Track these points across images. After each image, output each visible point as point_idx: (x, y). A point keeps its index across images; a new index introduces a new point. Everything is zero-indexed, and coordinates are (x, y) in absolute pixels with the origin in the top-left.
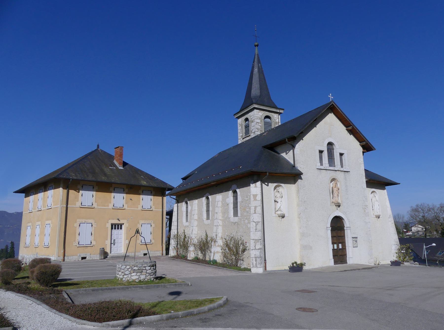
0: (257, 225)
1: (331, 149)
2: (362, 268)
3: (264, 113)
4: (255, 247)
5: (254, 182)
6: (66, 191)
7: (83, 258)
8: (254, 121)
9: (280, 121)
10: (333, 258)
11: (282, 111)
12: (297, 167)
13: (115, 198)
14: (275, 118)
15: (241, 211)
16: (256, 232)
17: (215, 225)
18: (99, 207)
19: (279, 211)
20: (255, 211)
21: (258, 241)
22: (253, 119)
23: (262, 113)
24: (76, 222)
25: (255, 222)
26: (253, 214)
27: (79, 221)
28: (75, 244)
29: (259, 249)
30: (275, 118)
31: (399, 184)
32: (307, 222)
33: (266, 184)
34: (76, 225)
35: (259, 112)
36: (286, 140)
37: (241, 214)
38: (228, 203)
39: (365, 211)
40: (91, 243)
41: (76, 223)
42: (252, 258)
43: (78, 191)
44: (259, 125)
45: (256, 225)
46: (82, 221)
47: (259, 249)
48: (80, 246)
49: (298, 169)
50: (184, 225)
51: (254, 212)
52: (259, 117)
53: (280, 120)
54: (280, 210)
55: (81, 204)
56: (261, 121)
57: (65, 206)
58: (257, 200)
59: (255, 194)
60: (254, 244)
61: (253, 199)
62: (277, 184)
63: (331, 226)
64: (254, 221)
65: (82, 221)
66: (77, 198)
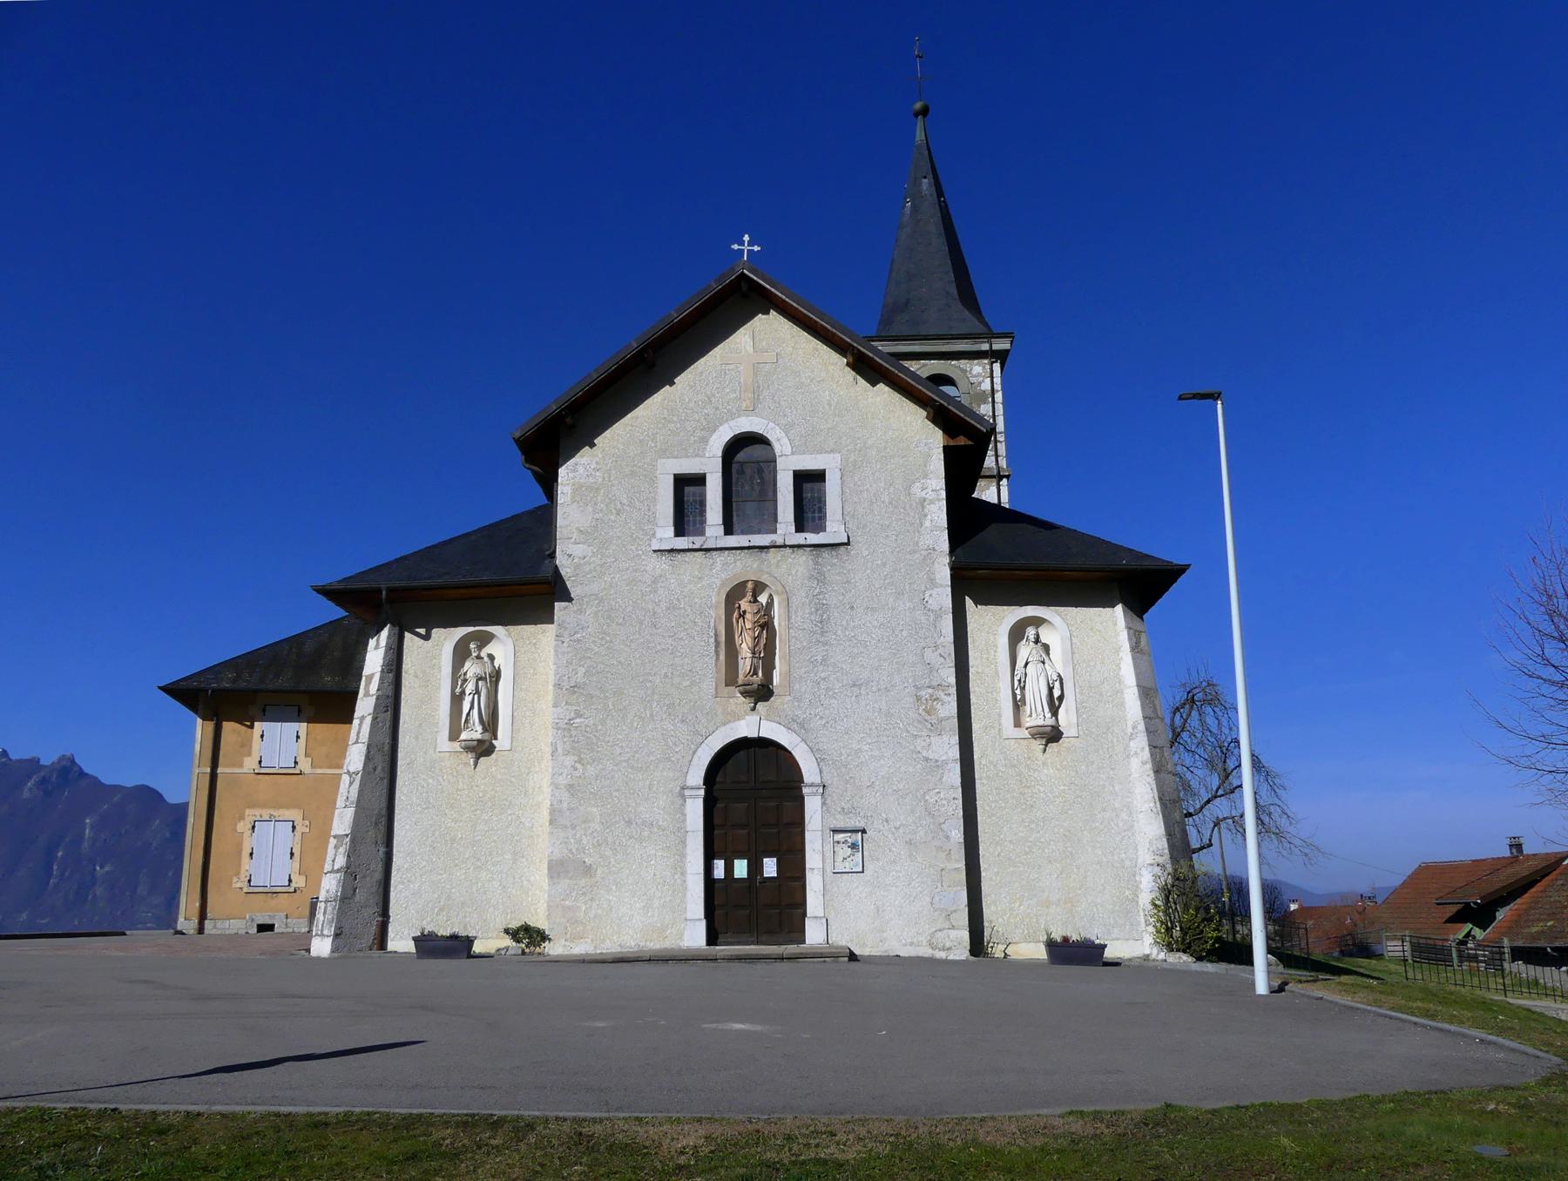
1: (758, 462)
2: (1316, 991)
6: (210, 725)
7: (265, 928)
9: (998, 387)
11: (1001, 345)
13: (264, 738)
14: (975, 376)
18: (319, 771)
24: (242, 818)
27: (251, 814)
28: (239, 885)
30: (975, 376)
33: (418, 635)
34: (244, 826)
40: (290, 881)
41: (242, 822)
43: (248, 723)
46: (261, 816)
48: (255, 892)
53: (998, 380)
55: (260, 762)
57: (209, 770)
62: (471, 629)
65: (261, 816)
66: (246, 747)
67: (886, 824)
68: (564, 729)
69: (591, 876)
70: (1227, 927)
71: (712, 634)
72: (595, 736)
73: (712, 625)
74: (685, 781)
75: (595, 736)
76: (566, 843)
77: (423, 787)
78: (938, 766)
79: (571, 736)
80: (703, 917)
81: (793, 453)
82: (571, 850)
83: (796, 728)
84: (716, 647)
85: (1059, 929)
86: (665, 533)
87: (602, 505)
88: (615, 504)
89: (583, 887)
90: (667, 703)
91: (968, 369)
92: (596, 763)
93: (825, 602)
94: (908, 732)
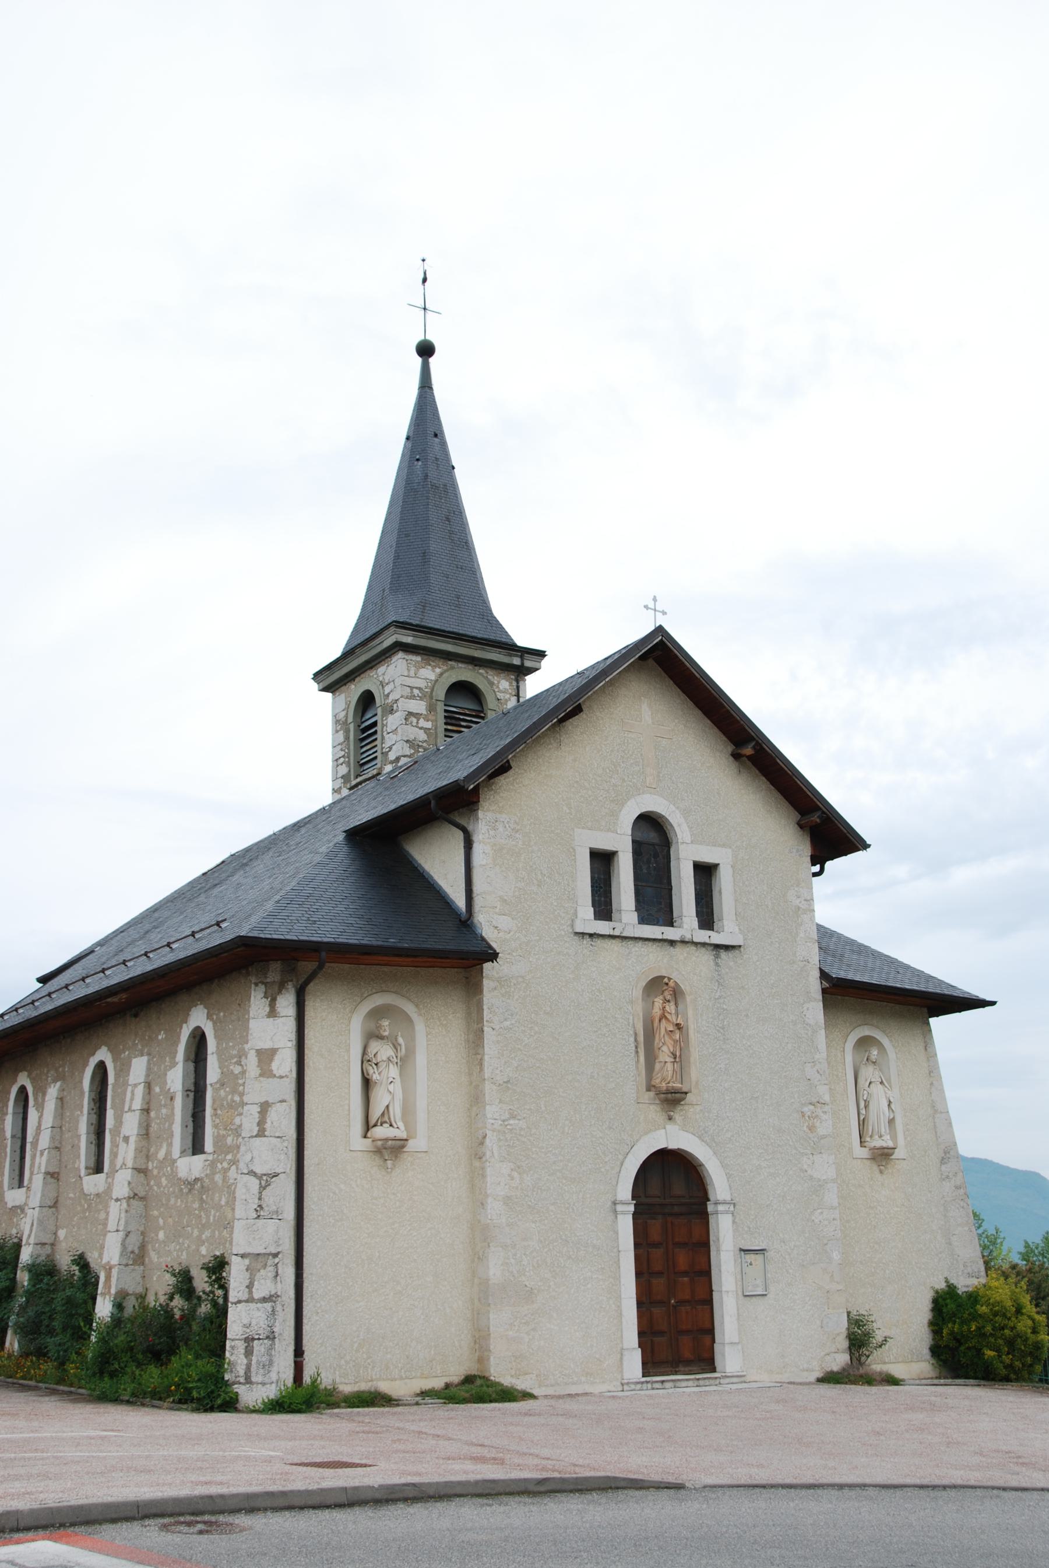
0: (264, 1189)
3: (445, 668)
4: (251, 1292)
5: (266, 993)
8: (395, 705)
10: (639, 1347)
12: (478, 925)
14: (499, 691)
15: (216, 1126)
16: (261, 1222)
17: (114, 1197)
19: (381, 1125)
20: (261, 1123)
21: (266, 1265)
22: (391, 697)
23: (438, 670)
25: (259, 1177)
26: (252, 1137)
29: (264, 1300)
31: (993, 1003)
32: (512, 1179)
35: (418, 668)
36: (430, 803)
37: (218, 1140)
38: (172, 1091)
39: (812, 1128)
42: (233, 1340)
44: (421, 728)
45: (262, 1188)
47: (264, 1300)
49: (483, 935)
50: (10, 1205)
51: (257, 1129)
52: (419, 689)
54: (386, 1122)
56: (431, 708)
58: (275, 1076)
59: (268, 1045)
60: (247, 1275)
61: (258, 1072)
63: (633, 1198)
64: (252, 1173)
67: (782, 1244)
68: (499, 1131)
69: (533, 1302)
70: (452, 1369)
71: (632, 1032)
72: (529, 1140)
73: (631, 1021)
74: (616, 1196)
75: (529, 1140)
76: (507, 1263)
77: (334, 1193)
78: (820, 1186)
79: (506, 1140)
80: (637, 1345)
81: (692, 842)
82: (512, 1272)
83: (708, 1141)
84: (636, 1047)
85: (899, 1350)
86: (585, 916)
87: (524, 873)
88: (535, 874)
89: (525, 1315)
90: (595, 1106)
91: (496, 682)
92: (532, 1172)
93: (725, 1007)
94: (796, 1149)
